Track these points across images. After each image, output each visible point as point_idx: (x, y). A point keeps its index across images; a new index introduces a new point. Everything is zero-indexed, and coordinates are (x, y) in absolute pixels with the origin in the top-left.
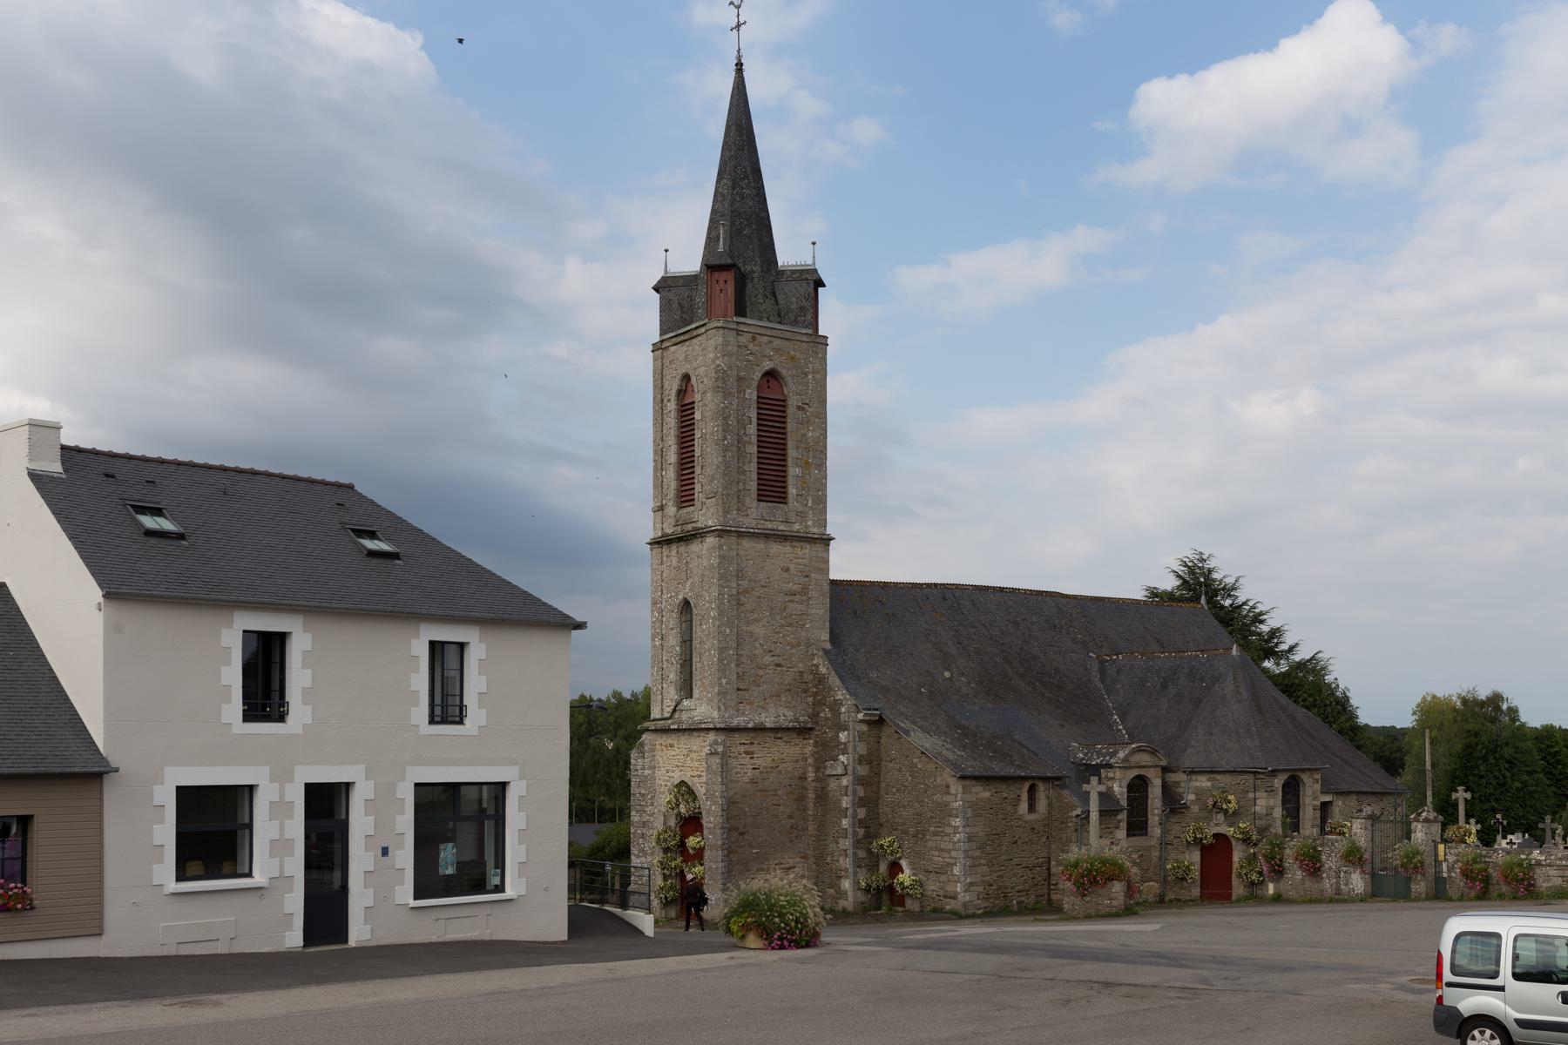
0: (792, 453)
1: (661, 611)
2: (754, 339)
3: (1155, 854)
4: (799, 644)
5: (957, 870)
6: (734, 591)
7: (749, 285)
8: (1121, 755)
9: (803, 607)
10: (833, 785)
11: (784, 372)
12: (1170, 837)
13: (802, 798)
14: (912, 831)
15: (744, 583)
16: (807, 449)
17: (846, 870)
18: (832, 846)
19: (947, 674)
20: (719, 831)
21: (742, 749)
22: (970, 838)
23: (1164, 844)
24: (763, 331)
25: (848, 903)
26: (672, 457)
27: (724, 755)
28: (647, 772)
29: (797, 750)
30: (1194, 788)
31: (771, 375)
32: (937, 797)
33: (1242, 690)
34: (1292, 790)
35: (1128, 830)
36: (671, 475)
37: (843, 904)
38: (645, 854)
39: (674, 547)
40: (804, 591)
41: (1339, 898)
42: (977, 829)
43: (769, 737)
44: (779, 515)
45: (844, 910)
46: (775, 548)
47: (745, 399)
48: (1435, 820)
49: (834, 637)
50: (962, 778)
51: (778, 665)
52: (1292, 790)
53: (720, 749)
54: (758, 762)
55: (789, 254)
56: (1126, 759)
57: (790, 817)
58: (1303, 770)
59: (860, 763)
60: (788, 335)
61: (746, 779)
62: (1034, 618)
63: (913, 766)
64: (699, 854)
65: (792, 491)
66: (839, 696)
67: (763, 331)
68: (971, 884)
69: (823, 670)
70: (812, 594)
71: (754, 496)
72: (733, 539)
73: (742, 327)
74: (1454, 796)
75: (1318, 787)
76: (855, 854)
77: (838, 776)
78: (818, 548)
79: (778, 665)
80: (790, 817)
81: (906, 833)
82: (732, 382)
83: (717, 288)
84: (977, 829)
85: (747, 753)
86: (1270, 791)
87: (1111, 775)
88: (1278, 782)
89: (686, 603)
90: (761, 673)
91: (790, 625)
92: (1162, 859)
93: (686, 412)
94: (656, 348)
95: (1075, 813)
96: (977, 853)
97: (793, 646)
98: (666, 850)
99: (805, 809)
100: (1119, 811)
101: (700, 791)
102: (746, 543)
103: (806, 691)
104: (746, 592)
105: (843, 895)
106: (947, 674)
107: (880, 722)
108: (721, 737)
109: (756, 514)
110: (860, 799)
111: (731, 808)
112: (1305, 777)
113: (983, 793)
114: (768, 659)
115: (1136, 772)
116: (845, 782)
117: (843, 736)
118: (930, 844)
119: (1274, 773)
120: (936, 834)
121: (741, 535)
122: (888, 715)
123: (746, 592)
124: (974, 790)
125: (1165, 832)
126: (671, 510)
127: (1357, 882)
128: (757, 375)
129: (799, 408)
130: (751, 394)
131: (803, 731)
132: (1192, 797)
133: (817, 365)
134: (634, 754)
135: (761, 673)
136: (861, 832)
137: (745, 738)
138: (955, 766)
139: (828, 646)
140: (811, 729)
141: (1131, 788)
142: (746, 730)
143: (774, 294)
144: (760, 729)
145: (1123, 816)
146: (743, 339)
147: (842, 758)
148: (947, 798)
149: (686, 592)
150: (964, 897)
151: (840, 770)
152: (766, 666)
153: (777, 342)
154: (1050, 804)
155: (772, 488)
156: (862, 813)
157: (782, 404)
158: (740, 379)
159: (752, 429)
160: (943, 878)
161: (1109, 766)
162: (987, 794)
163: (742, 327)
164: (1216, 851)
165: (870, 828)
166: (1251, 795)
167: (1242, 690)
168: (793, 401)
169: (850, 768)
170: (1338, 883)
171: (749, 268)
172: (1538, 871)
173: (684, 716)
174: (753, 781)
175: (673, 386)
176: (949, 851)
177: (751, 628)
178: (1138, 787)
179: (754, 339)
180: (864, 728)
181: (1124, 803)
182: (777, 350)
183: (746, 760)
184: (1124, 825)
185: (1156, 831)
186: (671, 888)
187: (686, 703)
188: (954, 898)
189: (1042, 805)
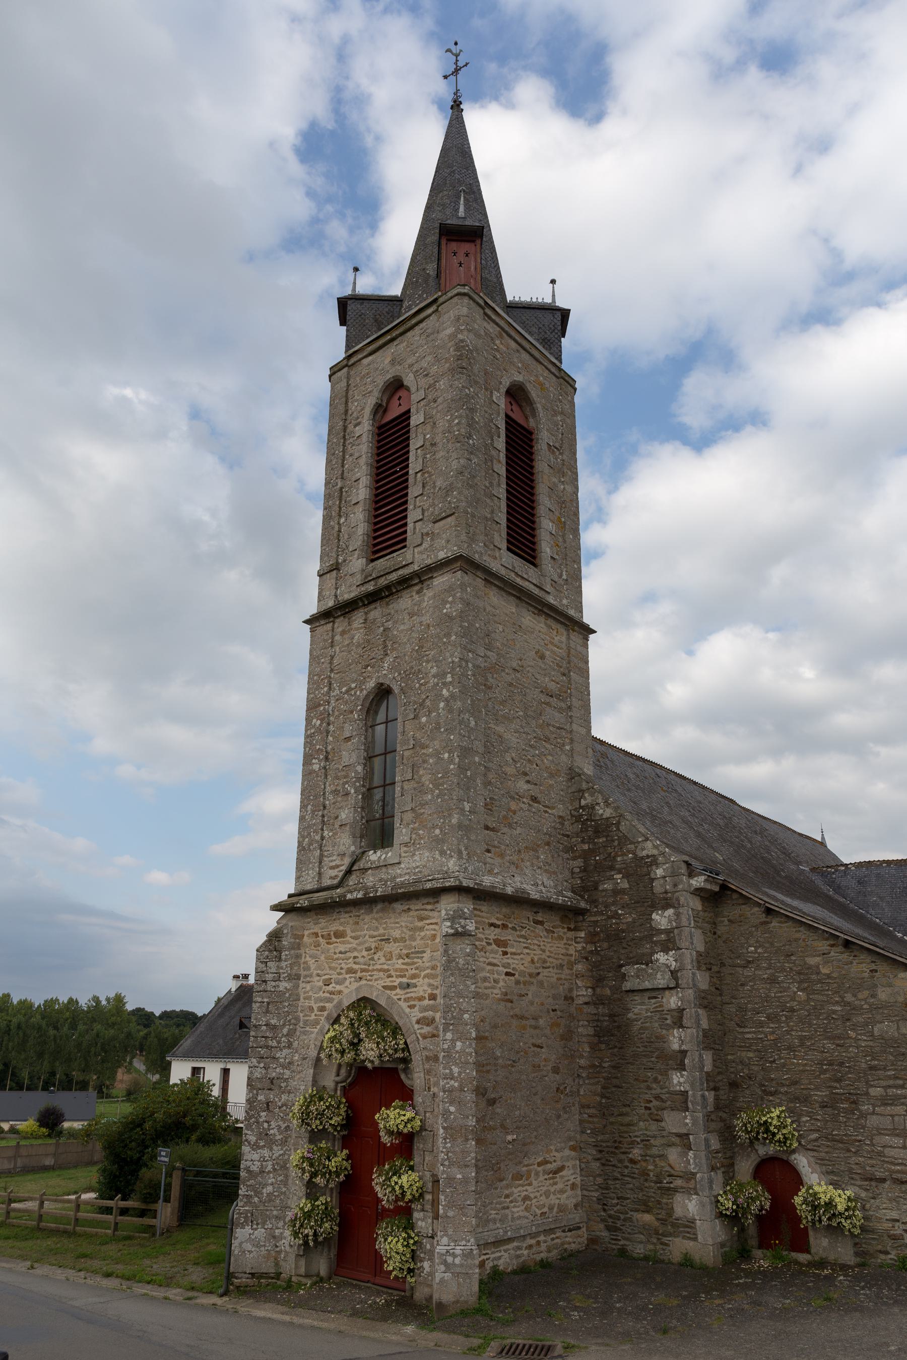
1: (326, 718)
10: (639, 1009)
14: (819, 1095)
17: (690, 1176)
18: (644, 1127)
20: (470, 1097)
21: (493, 934)
24: (513, 333)
26: (362, 492)
28: (284, 985)
37: (678, 1247)
38: (270, 1143)
39: (358, 618)
43: (525, 915)
45: (687, 1262)
46: (528, 619)
61: (497, 993)
64: (406, 1144)
66: (648, 849)
67: (513, 333)
77: (656, 992)
80: (556, 1070)
81: (806, 1100)
83: (455, 261)
85: (499, 943)
89: (383, 693)
93: (392, 439)
94: (334, 371)
97: (552, 776)
98: (315, 1137)
101: (408, 1015)
105: (688, 1227)
108: (467, 906)
114: (522, 786)
116: (673, 1001)
117: (662, 919)
135: (513, 806)
144: (519, 901)
147: (661, 957)
149: (385, 673)
151: (661, 980)
165: (729, 1090)
169: (686, 977)
173: (370, 879)
177: (500, 729)
186: (327, 1213)
187: (373, 856)
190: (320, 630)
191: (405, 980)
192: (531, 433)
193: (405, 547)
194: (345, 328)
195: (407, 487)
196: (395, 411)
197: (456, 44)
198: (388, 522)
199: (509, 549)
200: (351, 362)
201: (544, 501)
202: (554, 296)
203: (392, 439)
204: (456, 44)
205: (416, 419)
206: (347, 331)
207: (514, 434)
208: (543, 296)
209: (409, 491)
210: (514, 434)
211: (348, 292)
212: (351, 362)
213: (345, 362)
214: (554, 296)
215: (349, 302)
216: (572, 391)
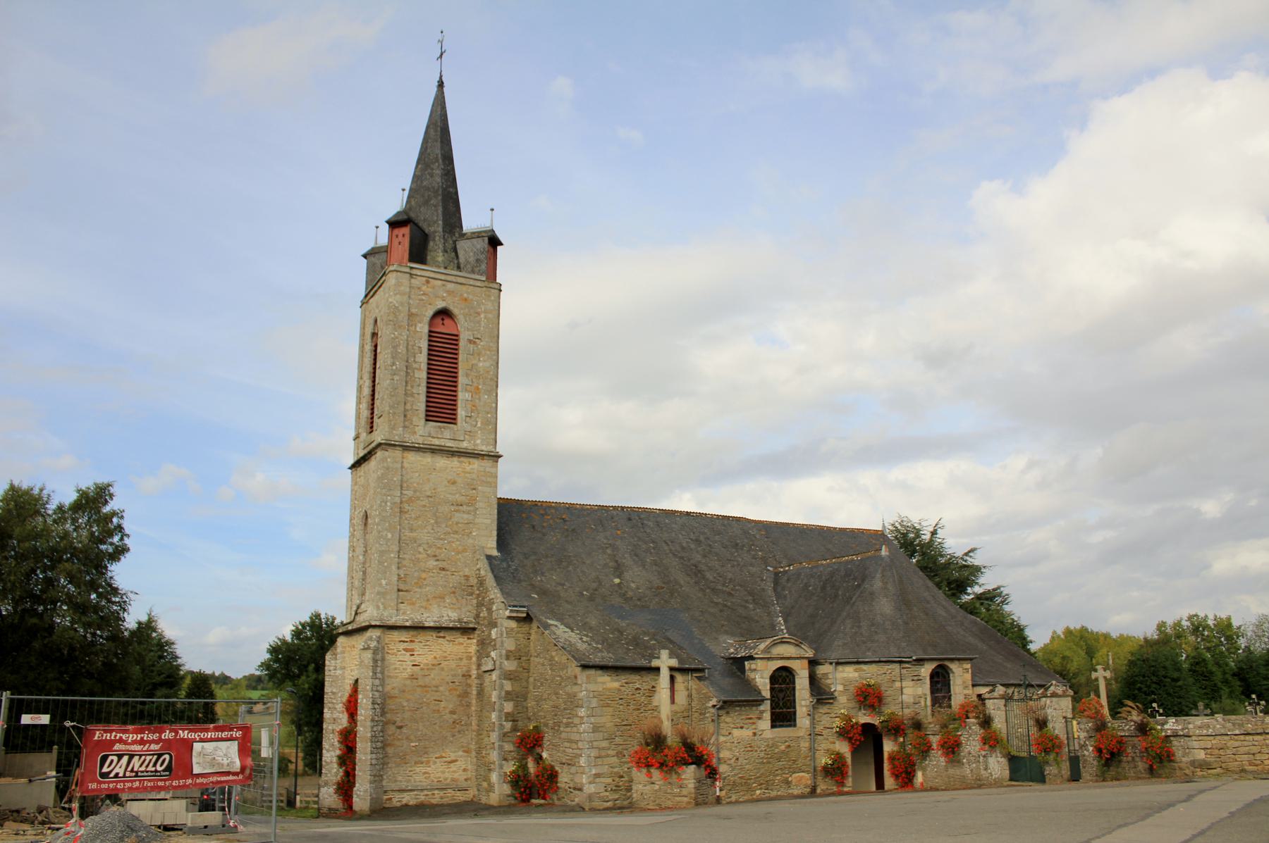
0: (462, 380)
2: (428, 282)
3: (805, 745)
4: (465, 550)
5: (583, 761)
6: (397, 500)
7: (431, 244)
8: (762, 646)
9: (471, 517)
11: (455, 311)
12: (819, 728)
13: (465, 694)
15: (410, 493)
16: (478, 377)
19: (617, 581)
22: (596, 729)
23: (813, 735)
25: (494, 799)
27: (375, 652)
28: (339, 672)
29: (462, 649)
30: (842, 679)
31: (444, 313)
32: (568, 689)
33: (890, 587)
34: (940, 680)
35: (773, 720)
36: (364, 406)
40: (472, 502)
41: (979, 784)
42: (603, 720)
44: (447, 434)
46: (441, 462)
47: (416, 332)
48: (1064, 695)
49: (502, 543)
50: (585, 667)
51: (444, 569)
52: (940, 680)
53: (373, 644)
54: (418, 659)
55: (472, 220)
56: (767, 650)
57: (453, 712)
58: (952, 660)
59: (508, 658)
60: (460, 280)
61: (405, 675)
62: (717, 538)
63: (552, 658)
65: (461, 413)
68: (597, 775)
69: (482, 573)
70: (479, 505)
71: (422, 415)
72: (398, 453)
73: (414, 272)
74: (1094, 675)
75: (968, 676)
76: (501, 747)
78: (487, 464)
79: (444, 569)
80: (453, 712)
82: (403, 317)
84: (603, 720)
85: (406, 650)
86: (917, 679)
87: (753, 666)
88: (926, 670)
90: (424, 575)
91: (456, 532)
92: (812, 749)
95: (711, 704)
96: (605, 744)
99: (469, 705)
100: (763, 700)
102: (412, 457)
103: (471, 594)
104: (410, 500)
106: (617, 581)
107: (528, 619)
109: (423, 431)
110: (508, 693)
111: (382, 706)
112: (953, 666)
113: (609, 682)
115: (780, 663)
117: (494, 633)
118: (563, 735)
119: (920, 661)
120: (567, 725)
121: (406, 448)
122: (535, 612)
123: (410, 500)
124: (600, 679)
125: (813, 724)
126: (364, 435)
127: (997, 766)
128: (430, 313)
129: (470, 341)
130: (423, 328)
131: (466, 631)
132: (840, 688)
133: (490, 306)
134: (328, 656)
135: (424, 575)
136: (508, 725)
137: (404, 636)
138: (574, 653)
139: (495, 553)
140: (474, 629)
141: (773, 679)
142: (406, 627)
143: (455, 250)
144: (419, 628)
145: (767, 706)
146: (415, 282)
148: (576, 689)
150: (590, 789)
151: (490, 667)
152: (430, 570)
153: (450, 286)
154: (690, 696)
155: (441, 406)
156: (509, 707)
157: (454, 339)
158: (411, 315)
159: (423, 358)
160: (573, 769)
161: (751, 658)
162: (616, 685)
163: (414, 272)
164: (867, 740)
166: (898, 684)
167: (890, 587)
168: (464, 337)
170: (978, 768)
171: (432, 229)
172: (1175, 742)
174: (413, 677)
175: (369, 331)
176: (576, 742)
178: (782, 678)
179: (428, 282)
180: (513, 624)
181: (766, 693)
182: (450, 292)
183: (407, 656)
184: (767, 715)
185: (803, 720)
188: (580, 790)
189: (681, 697)
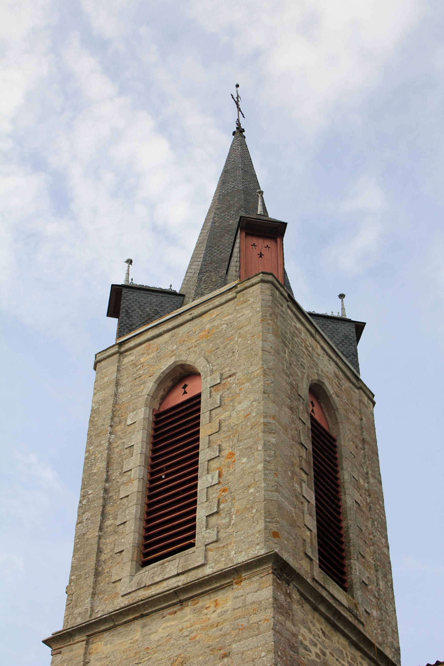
93: (175, 433)
190: (67, 653)
191: (193, 641)
192: (335, 440)
193: (193, 545)
194: (115, 321)
195: (196, 478)
196: (178, 397)
197: (261, 255)
198: (168, 523)
199: (320, 567)
200: (123, 349)
201: (350, 497)
202: (343, 309)
203: (175, 433)
204: (261, 255)
205: (205, 405)
206: (119, 323)
207: (335, 544)
208: (332, 309)
209: (200, 482)
210: (335, 544)
211: (121, 281)
212: (123, 349)
213: (116, 349)
214: (343, 309)
215: (124, 290)
216: (371, 404)
